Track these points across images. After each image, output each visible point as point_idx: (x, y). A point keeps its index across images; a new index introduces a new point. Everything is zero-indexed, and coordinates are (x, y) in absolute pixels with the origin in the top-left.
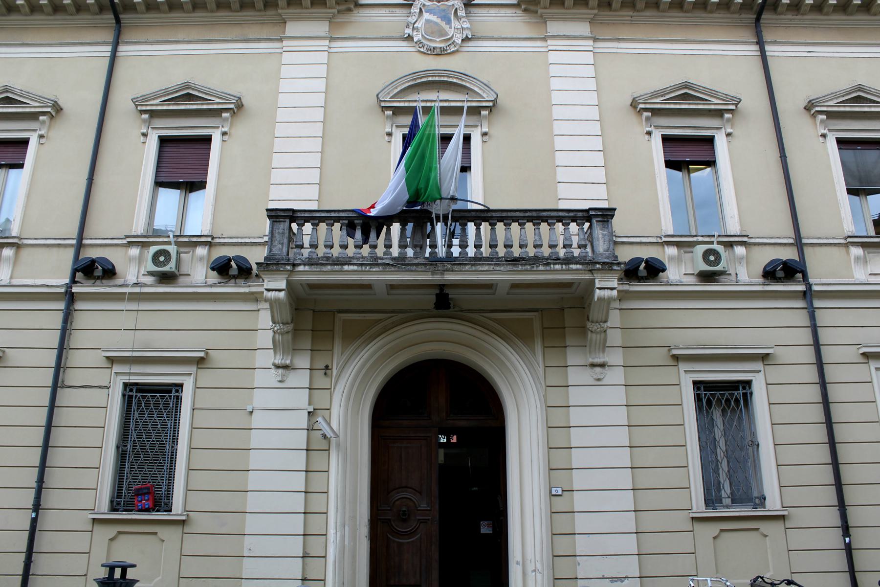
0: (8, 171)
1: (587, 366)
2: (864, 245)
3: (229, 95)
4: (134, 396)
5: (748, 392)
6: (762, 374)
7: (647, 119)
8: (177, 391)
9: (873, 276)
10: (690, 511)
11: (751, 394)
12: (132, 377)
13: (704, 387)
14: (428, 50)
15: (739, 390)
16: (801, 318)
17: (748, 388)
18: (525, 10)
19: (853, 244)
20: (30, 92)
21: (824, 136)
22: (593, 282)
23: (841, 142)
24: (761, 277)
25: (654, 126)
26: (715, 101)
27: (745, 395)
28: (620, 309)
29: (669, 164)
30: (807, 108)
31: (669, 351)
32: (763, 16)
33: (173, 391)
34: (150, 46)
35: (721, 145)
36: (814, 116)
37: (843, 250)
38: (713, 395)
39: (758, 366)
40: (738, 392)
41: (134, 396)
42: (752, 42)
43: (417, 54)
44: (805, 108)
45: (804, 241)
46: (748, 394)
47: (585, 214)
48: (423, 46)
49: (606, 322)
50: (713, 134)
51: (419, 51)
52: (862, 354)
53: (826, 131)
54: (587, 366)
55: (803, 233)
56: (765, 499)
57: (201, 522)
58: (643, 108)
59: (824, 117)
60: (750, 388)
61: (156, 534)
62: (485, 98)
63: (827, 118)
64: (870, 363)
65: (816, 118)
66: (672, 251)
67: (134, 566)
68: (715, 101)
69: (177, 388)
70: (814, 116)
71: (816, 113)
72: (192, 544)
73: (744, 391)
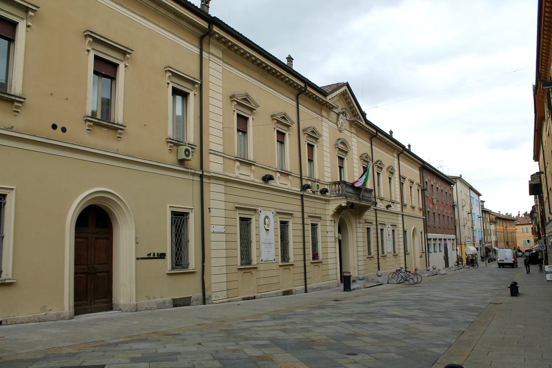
0: (102, 79)
2: (240, 162)
5: (3, 202)
6: (254, 216)
7: (89, 42)
8: (186, 216)
11: (5, 203)
13: (174, 214)
15: (184, 216)
16: (299, 203)
17: (3, 199)
18: (350, 123)
19: (238, 160)
21: (88, 51)
22: (371, 206)
23: (96, 57)
25: (171, 81)
26: (318, 135)
29: (95, 73)
31: (276, 210)
32: (206, 37)
33: (185, 215)
34: (487, 209)
35: (121, 71)
36: (232, 101)
37: (233, 162)
44: (230, 97)
45: (303, 177)
46: (3, 203)
49: (340, 209)
51: (338, 130)
52: (235, 207)
53: (90, 48)
55: (303, 175)
56: (189, 264)
57: (261, 267)
58: (235, 100)
59: (91, 40)
60: (4, 199)
63: (237, 104)
64: (237, 211)
65: (87, 38)
68: (318, 135)
70: (232, 101)
71: (87, 35)
72: (261, 274)
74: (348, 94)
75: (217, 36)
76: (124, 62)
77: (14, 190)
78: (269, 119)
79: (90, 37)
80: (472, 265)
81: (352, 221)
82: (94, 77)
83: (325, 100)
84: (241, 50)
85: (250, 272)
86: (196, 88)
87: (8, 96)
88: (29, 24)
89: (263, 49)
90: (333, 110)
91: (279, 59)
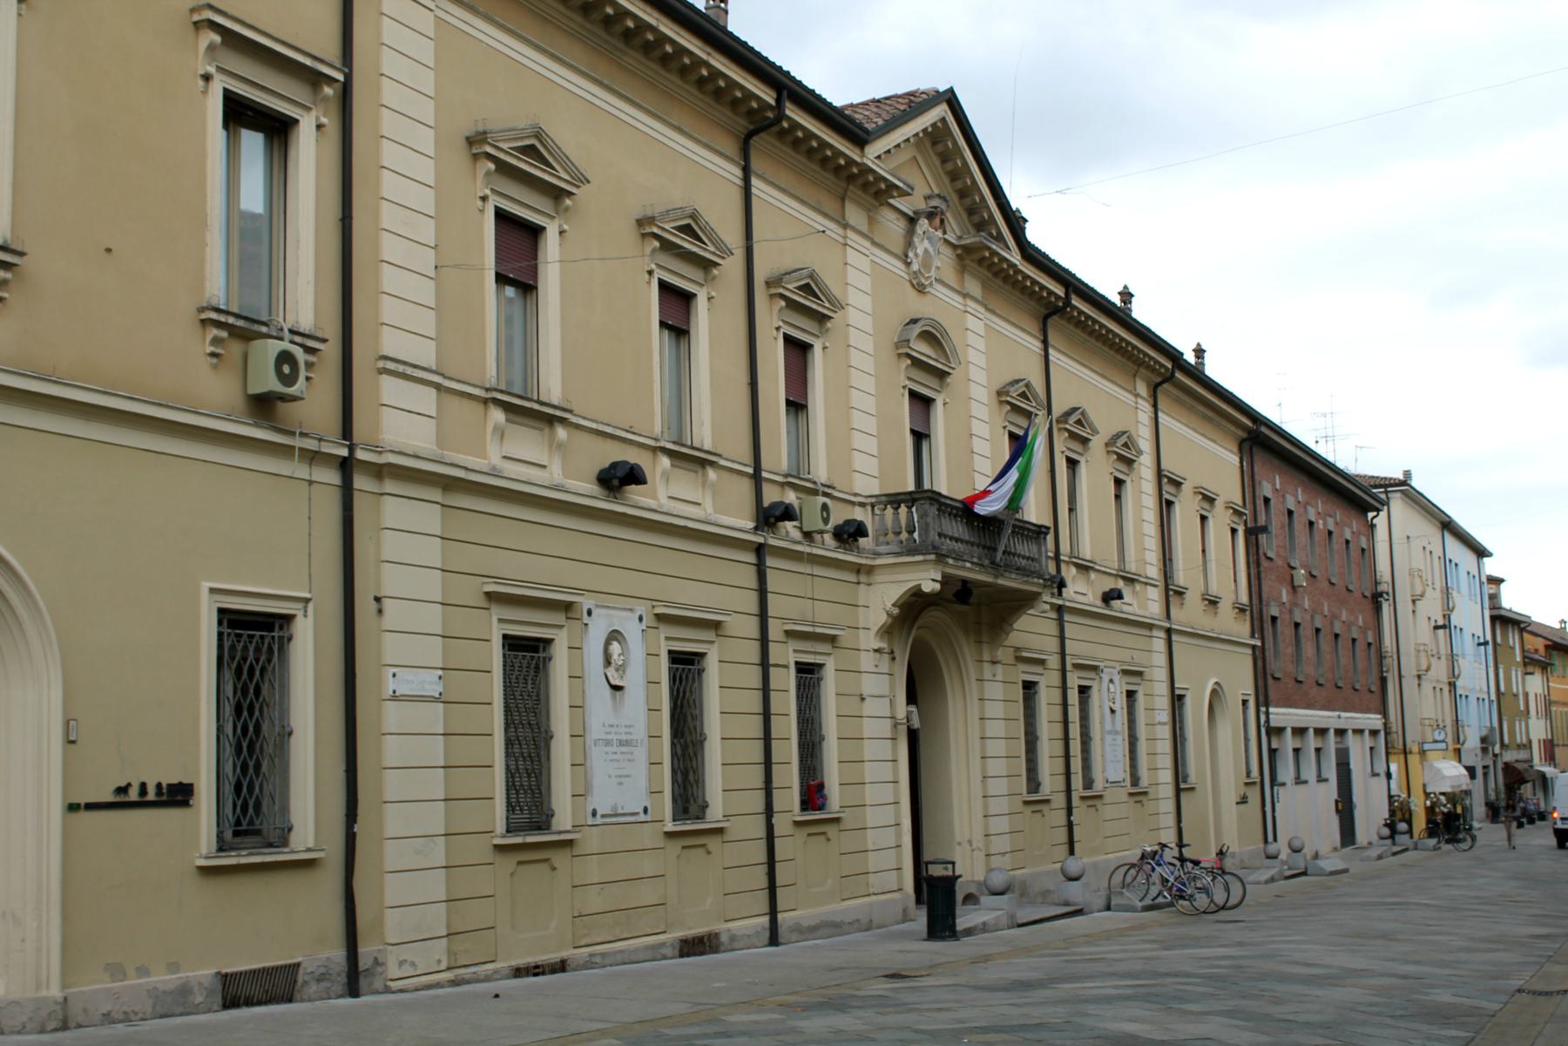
1: (868, 651)
2: (508, 408)
3: (721, 240)
4: (226, 634)
8: (281, 628)
9: (672, 500)
10: (492, 834)
12: (818, 657)
14: (918, 284)
16: (749, 577)
19: (497, 402)
20: (715, 230)
22: (1039, 594)
24: (595, 481)
27: (281, 638)
28: (443, 505)
30: (471, 140)
38: (677, 669)
39: (559, 618)
40: (536, 655)
41: (226, 634)
42: (739, 164)
43: (908, 284)
47: (1037, 529)
48: (917, 277)
50: (545, 225)
53: (211, 70)
54: (868, 651)
61: (547, 860)
62: (950, 362)
66: (665, 461)
67: (1424, 786)
68: (827, 305)
69: (281, 621)
70: (475, 157)
72: (593, 870)
73: (281, 634)
78: (630, 235)
86: (326, 99)
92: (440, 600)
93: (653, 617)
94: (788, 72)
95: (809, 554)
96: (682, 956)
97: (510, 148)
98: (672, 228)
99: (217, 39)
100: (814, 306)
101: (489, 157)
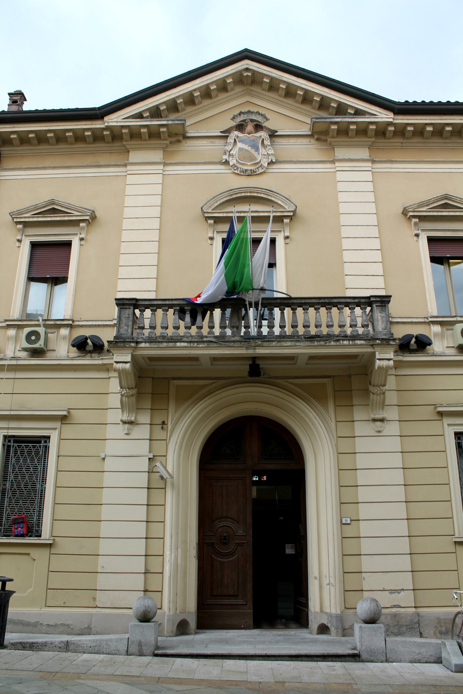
1: (369, 421)
2: (441, 323)
8: (45, 442)
14: (241, 172)
18: (318, 139)
22: (374, 354)
25: (421, 230)
28: (396, 375)
29: (434, 260)
33: (43, 442)
47: (367, 300)
51: (234, 173)
54: (369, 421)
69: (46, 439)
71: (411, 217)
74: (265, 75)
75: (449, 129)
76: (282, 232)
77: (57, 429)
78: (403, 222)
79: (414, 218)
80: (442, 646)
81: (308, 417)
82: (432, 267)
83: (103, 126)
84: (388, 128)
85: (28, 554)
86: (287, 224)
87: (378, 321)
88: (287, 234)
89: (78, 108)
90: (276, 134)
91: (42, 109)
92: (398, 419)
93: (436, 414)
94: (448, 102)
95: (8, 365)
96: (177, 635)
97: (212, 210)
98: (212, 210)
99: (417, 220)
100: (66, 218)
101: (414, 217)
